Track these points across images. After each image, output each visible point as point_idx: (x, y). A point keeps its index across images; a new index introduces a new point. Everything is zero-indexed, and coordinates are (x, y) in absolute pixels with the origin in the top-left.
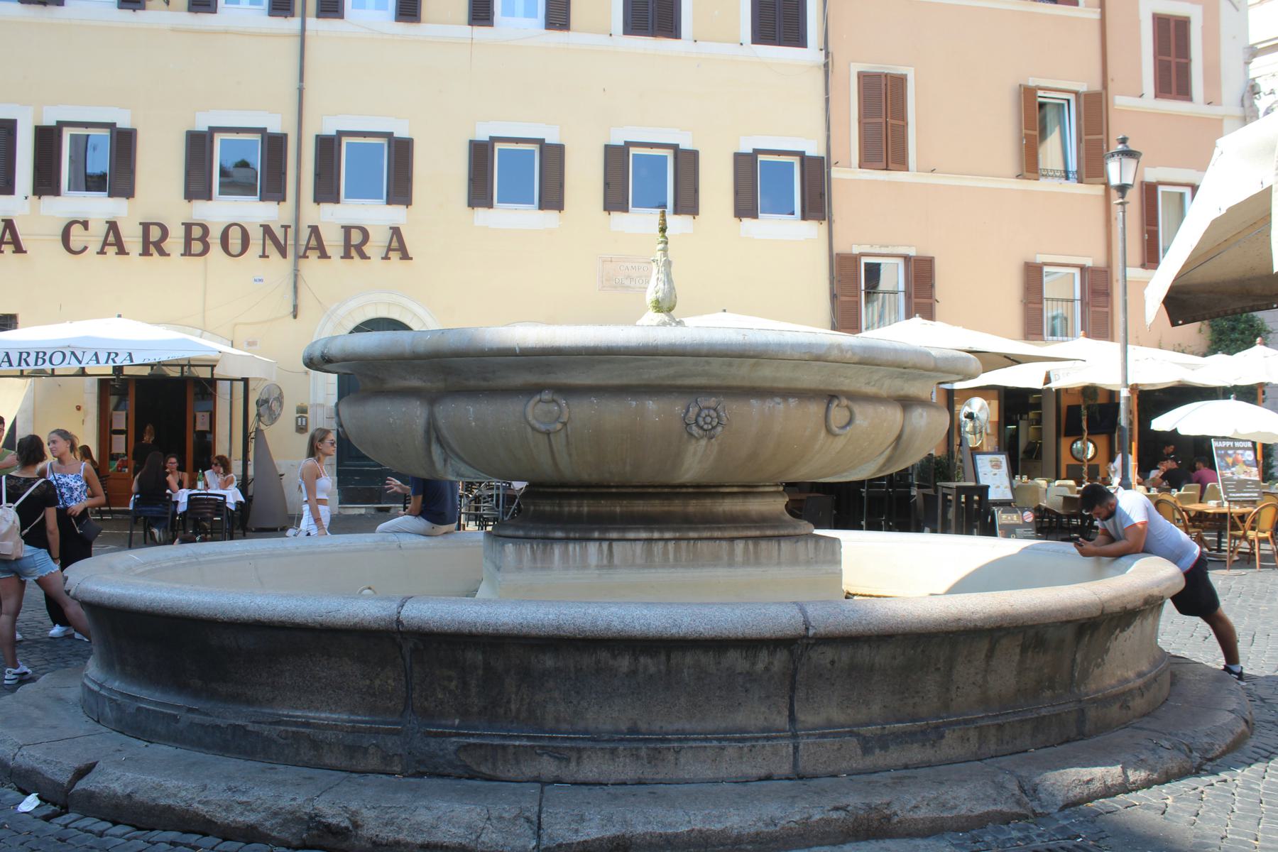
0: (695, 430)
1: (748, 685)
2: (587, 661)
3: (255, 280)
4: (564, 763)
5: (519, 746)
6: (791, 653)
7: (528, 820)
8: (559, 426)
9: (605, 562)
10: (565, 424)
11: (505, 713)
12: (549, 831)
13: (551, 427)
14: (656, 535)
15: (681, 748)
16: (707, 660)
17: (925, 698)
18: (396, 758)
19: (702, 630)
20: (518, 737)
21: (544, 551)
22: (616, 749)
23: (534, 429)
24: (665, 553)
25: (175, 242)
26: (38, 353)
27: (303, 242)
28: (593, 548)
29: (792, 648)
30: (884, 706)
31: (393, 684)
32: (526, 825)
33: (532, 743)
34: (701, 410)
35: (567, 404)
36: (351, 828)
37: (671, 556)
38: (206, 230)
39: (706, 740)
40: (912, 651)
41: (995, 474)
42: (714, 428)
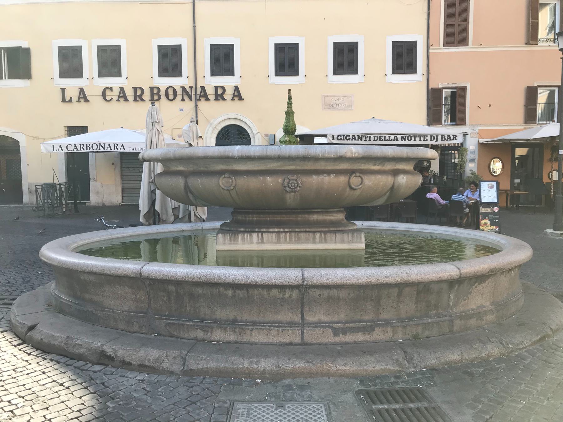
0: (288, 189)
1: (283, 304)
2: (215, 291)
3: (180, 110)
4: (206, 333)
5: (189, 325)
6: (300, 291)
7: (182, 357)
8: (232, 188)
9: (260, 241)
10: (234, 187)
11: (185, 310)
12: (188, 363)
13: (229, 189)
14: (281, 230)
15: (253, 329)
16: (264, 292)
17: (367, 312)
18: (144, 327)
19: (257, 281)
20: (189, 321)
21: (235, 236)
22: (227, 328)
23: (223, 189)
24: (286, 238)
25: (147, 96)
26: (87, 144)
27: (199, 93)
28: (255, 235)
29: (300, 289)
30: (346, 315)
31: (144, 297)
32: (181, 359)
33: (194, 324)
34: (290, 181)
35: (235, 178)
36: (115, 357)
37: (288, 239)
38: (159, 90)
39: (264, 326)
40: (358, 292)
41: (489, 191)
42: (296, 188)
